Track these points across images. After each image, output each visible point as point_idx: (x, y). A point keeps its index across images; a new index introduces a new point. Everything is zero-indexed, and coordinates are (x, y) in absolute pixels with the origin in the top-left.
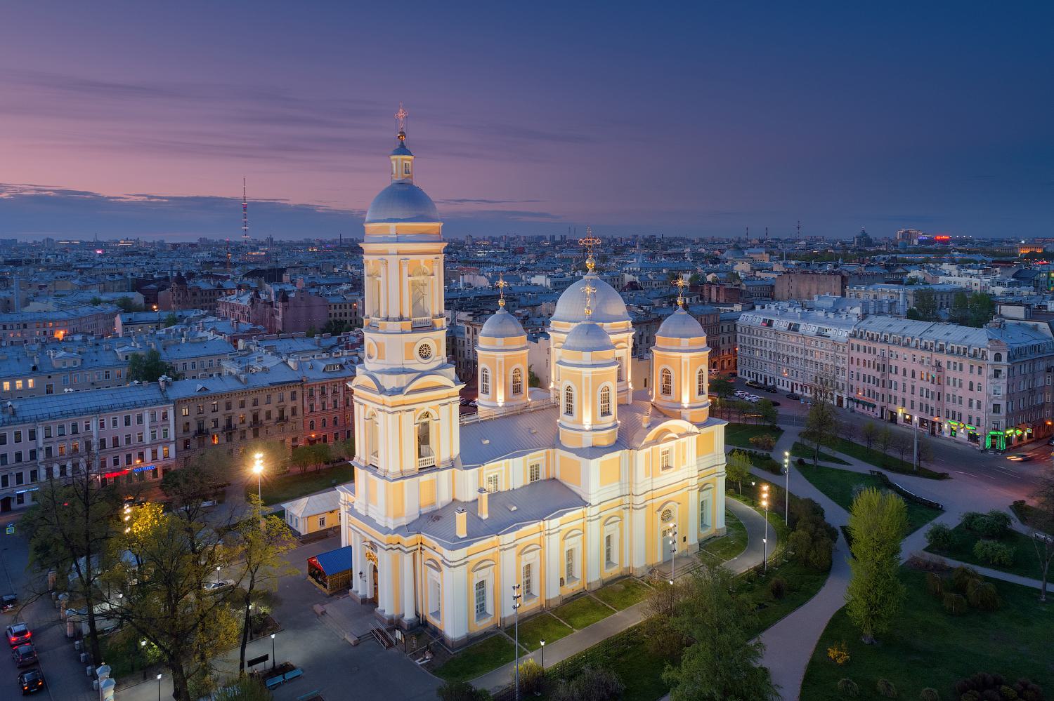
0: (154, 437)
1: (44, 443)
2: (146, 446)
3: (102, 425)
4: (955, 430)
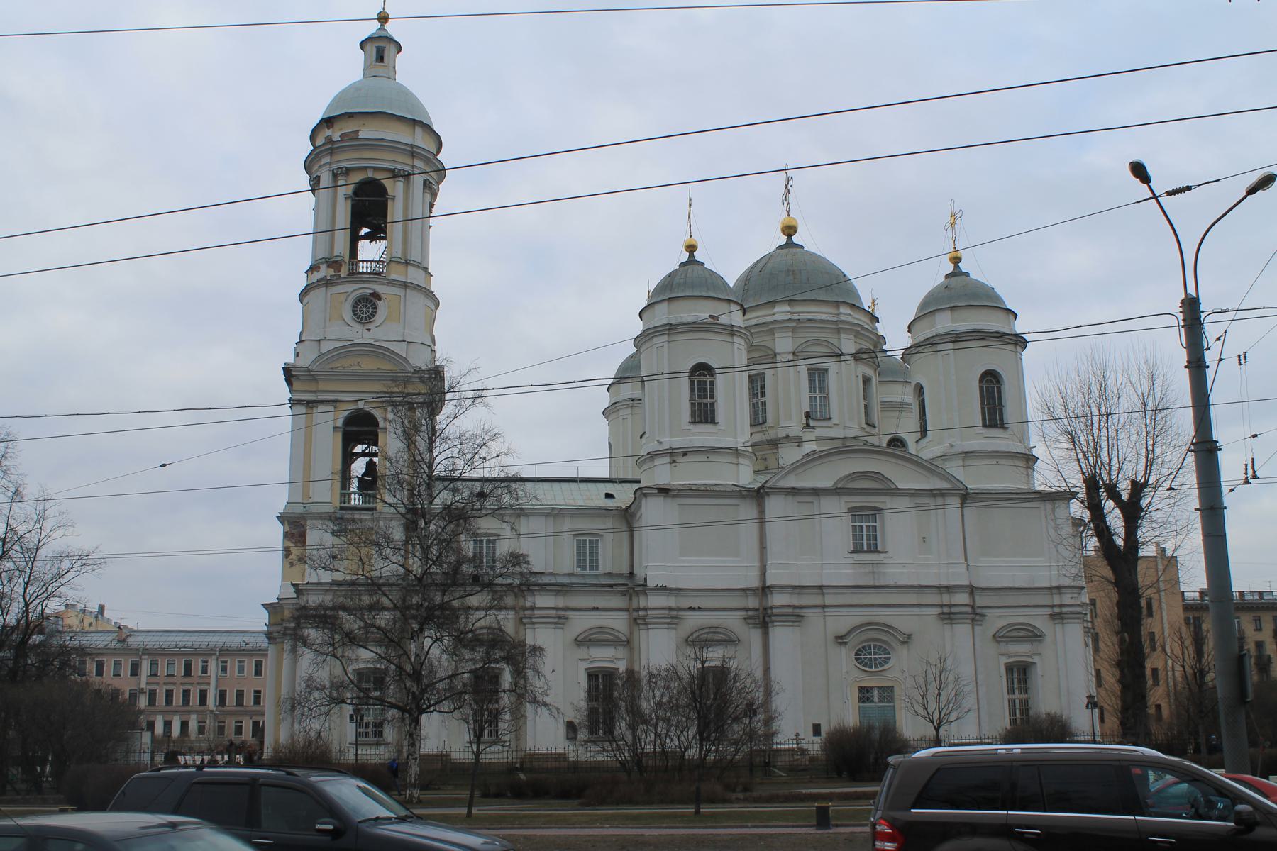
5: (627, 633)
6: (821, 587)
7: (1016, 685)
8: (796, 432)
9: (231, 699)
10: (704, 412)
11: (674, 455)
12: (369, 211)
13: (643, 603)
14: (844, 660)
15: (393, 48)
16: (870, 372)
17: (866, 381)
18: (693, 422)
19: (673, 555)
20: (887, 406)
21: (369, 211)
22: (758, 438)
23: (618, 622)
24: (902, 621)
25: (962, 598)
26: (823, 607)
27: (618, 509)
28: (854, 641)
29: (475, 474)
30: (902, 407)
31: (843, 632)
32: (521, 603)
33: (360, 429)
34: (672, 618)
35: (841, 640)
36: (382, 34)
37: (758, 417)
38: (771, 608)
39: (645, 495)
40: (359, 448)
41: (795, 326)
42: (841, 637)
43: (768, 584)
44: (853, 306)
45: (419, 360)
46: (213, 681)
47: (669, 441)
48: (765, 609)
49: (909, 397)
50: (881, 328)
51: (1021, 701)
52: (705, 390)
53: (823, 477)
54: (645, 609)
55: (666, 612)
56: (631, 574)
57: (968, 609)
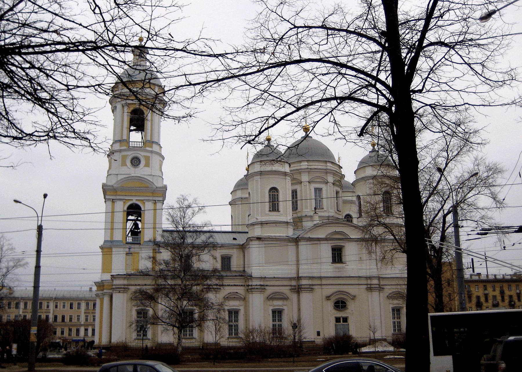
0: (87, 320)
1: (23, 312)
2: (81, 325)
3: (56, 307)
4: (309, 334)
5: (244, 295)
7: (396, 316)
9: (59, 319)
10: (274, 207)
11: (262, 224)
13: (250, 283)
14: (329, 306)
16: (339, 189)
17: (337, 193)
18: (270, 211)
19: (260, 263)
20: (345, 202)
21: (138, 122)
23: (241, 290)
24: (352, 290)
25: (375, 282)
26: (321, 285)
27: (239, 245)
28: (334, 299)
30: (352, 202)
31: (329, 294)
34: (262, 288)
35: (328, 298)
37: (295, 208)
38: (301, 285)
39: (252, 240)
40: (130, 217)
41: (309, 171)
42: (329, 297)
43: (300, 275)
44: (332, 163)
45: (159, 185)
46: (51, 311)
47: (261, 219)
48: (298, 286)
49: (354, 199)
51: (398, 322)
52: (275, 198)
53: (322, 233)
54: (251, 285)
55: (260, 287)
56: (244, 270)
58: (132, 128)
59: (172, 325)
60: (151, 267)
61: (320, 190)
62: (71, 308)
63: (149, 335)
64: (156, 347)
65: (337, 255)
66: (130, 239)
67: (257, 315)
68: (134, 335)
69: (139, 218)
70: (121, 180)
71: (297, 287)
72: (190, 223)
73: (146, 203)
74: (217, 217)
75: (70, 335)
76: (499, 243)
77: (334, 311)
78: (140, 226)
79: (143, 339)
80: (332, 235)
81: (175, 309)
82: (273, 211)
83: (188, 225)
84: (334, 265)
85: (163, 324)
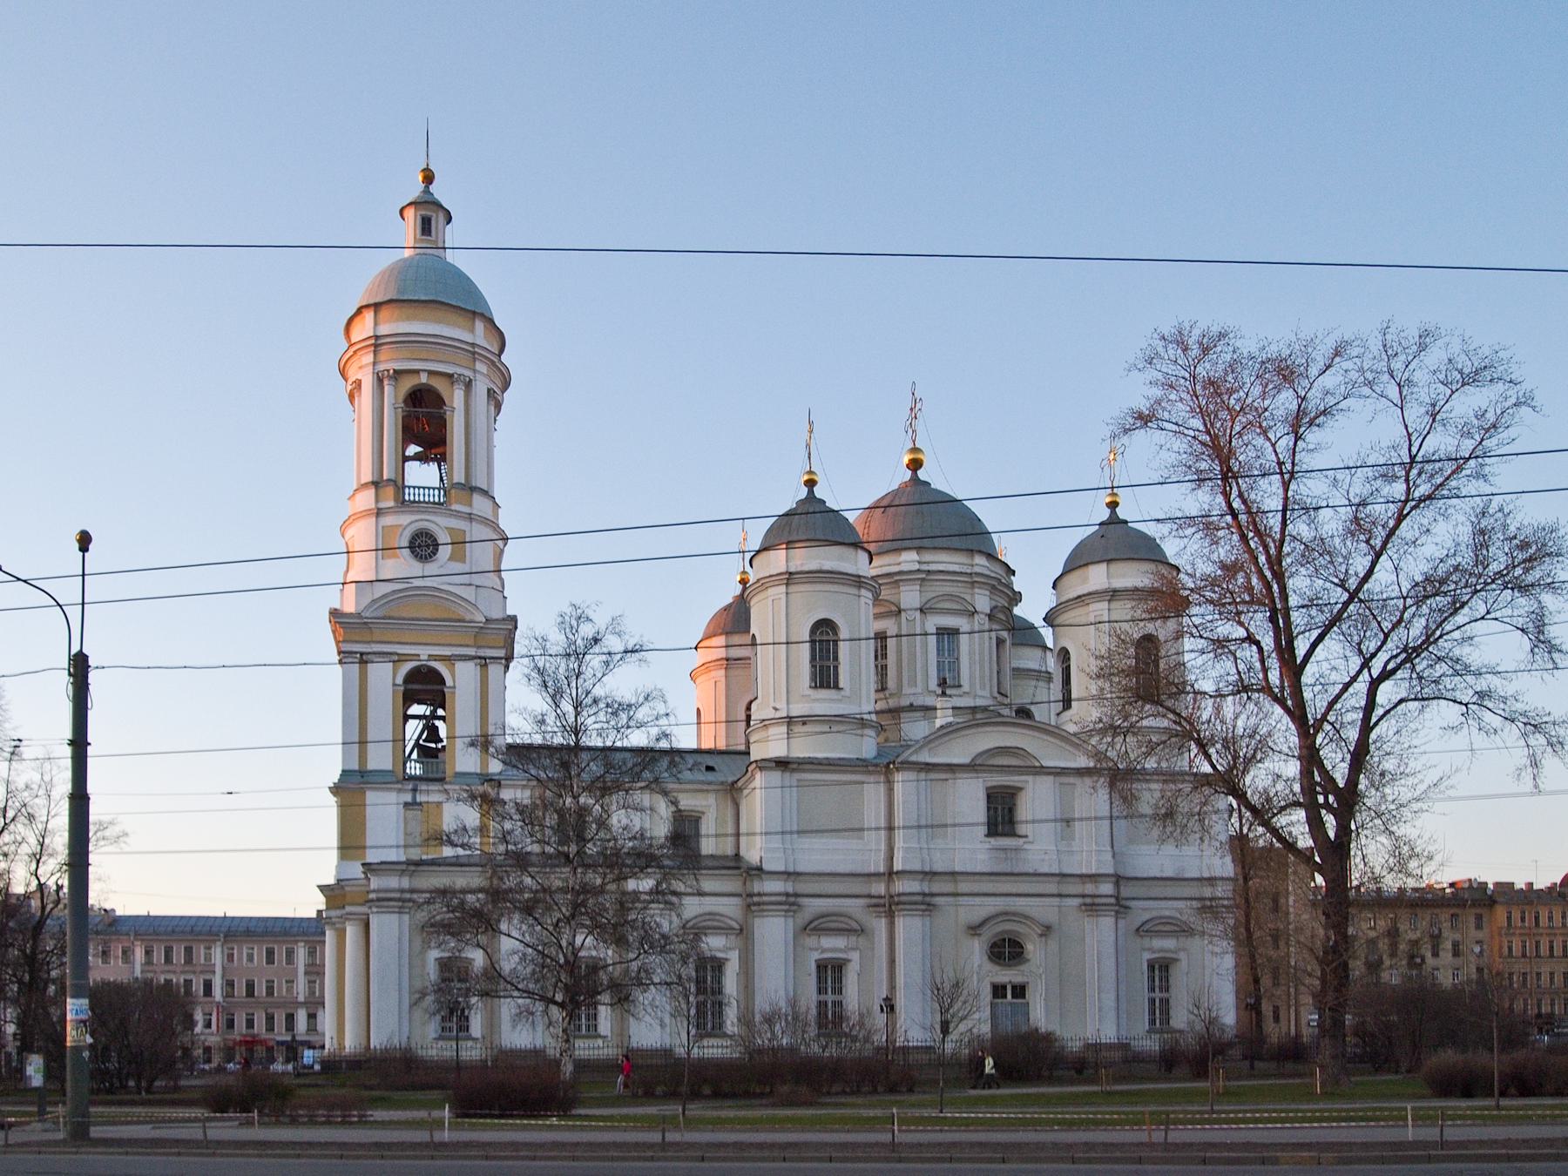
2: (299, 1005)
3: (230, 957)
6: (953, 874)
8: (929, 701)
9: (239, 989)
12: (423, 422)
14: (976, 951)
15: (442, 218)
22: (881, 705)
25: (1107, 888)
28: (989, 933)
29: (626, 743)
32: (749, 889)
33: (425, 686)
35: (974, 930)
36: (427, 198)
40: (417, 709)
49: (1052, 664)
50: (1018, 584)
53: (959, 751)
54: (759, 895)
55: (919, 898)
56: (737, 855)
57: (1113, 900)
58: (413, 449)
59: (542, 998)
60: (477, 822)
61: (953, 633)
62: (270, 961)
63: (476, 1026)
64: (495, 1060)
65: (1002, 815)
66: (414, 768)
67: (771, 975)
68: (432, 1029)
69: (440, 712)
70: (384, 596)
71: (886, 901)
72: (598, 691)
73: (459, 665)
74: (669, 698)
75: (270, 1028)
76: (1530, 770)
77: (988, 966)
78: (443, 733)
79: (457, 1039)
80: (993, 756)
81: (553, 951)
82: (822, 686)
83: (589, 700)
84: (992, 840)
85: (516, 993)
